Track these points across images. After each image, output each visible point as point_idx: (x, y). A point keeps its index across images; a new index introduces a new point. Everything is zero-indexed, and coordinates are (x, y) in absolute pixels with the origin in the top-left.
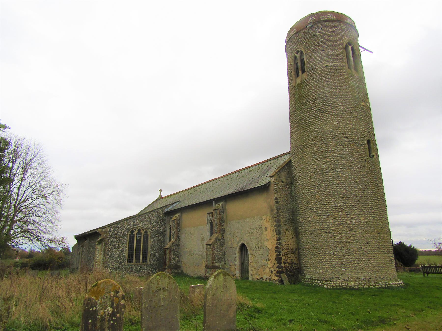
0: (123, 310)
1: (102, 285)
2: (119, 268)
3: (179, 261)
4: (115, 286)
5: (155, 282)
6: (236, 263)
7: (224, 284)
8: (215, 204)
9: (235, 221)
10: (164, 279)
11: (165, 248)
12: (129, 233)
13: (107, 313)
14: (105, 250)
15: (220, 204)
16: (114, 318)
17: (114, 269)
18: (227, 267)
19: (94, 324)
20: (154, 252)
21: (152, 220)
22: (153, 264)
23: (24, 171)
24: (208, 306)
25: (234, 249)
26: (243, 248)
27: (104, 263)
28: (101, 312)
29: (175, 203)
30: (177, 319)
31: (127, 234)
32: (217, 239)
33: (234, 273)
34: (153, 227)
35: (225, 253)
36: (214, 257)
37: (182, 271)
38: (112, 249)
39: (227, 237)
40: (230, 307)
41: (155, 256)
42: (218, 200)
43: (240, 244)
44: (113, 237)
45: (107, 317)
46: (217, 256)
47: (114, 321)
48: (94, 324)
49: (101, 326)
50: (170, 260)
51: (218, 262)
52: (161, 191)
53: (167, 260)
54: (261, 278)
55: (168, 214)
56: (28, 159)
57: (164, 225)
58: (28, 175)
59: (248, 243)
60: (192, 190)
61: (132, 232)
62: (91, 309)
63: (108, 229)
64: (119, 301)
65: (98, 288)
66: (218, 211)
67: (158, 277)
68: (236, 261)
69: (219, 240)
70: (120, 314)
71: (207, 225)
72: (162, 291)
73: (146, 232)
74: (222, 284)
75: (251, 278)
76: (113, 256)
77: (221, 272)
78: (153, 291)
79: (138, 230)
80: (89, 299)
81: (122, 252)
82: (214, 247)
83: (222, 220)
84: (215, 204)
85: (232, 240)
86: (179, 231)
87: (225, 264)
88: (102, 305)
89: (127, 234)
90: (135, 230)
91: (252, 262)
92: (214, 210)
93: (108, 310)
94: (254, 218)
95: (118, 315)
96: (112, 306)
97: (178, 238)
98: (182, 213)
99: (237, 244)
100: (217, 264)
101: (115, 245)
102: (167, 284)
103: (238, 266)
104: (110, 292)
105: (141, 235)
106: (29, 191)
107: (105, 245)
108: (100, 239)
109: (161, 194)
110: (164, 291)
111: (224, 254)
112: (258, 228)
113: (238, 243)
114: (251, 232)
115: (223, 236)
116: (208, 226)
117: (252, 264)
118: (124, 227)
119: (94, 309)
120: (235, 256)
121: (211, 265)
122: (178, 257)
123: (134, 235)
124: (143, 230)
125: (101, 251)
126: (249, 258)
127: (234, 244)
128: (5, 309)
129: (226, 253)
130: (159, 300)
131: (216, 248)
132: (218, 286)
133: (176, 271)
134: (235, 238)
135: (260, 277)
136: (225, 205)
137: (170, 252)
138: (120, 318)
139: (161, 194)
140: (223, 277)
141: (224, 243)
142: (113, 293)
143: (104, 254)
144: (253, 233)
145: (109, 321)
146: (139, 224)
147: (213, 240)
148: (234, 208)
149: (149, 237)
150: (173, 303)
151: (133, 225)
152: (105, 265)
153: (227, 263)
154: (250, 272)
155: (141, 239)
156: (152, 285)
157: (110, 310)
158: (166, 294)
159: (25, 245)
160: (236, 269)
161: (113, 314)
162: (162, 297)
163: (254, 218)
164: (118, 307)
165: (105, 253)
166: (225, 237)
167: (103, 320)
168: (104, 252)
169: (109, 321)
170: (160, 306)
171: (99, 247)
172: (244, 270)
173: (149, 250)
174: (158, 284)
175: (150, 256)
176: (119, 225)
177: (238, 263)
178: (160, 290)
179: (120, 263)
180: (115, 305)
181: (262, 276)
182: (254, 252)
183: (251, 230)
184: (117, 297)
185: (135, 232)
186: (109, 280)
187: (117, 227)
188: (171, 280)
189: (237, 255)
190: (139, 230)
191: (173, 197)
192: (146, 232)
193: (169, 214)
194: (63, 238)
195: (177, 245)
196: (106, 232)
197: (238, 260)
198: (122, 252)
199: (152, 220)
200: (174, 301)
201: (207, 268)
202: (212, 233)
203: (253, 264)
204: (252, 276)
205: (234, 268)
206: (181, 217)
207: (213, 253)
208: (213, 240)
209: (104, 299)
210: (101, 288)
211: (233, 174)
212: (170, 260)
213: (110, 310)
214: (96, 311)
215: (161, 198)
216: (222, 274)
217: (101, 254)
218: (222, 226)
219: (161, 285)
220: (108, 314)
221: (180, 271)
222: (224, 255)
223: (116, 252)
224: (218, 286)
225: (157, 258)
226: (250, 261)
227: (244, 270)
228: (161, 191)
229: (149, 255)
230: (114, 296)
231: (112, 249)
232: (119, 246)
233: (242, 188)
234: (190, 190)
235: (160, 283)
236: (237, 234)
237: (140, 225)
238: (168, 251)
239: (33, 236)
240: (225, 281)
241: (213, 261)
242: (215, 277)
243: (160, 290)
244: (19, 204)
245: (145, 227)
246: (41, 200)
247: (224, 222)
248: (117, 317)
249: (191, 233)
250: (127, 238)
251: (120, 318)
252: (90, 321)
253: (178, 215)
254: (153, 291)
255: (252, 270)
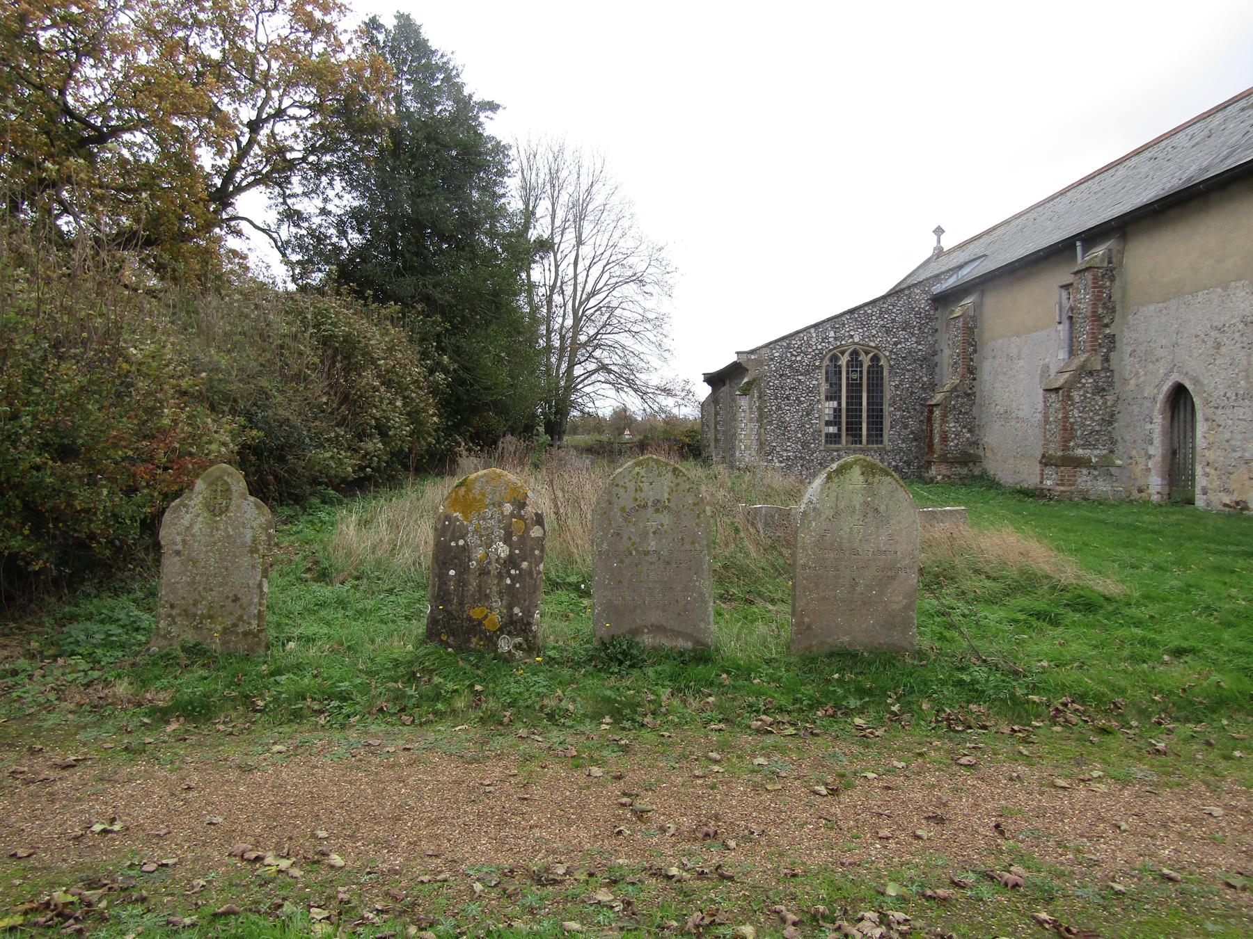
0: (537, 552)
1: (478, 486)
2: (801, 458)
3: (976, 443)
4: (515, 489)
5: (628, 484)
6: (1152, 451)
7: (866, 503)
8: (1085, 251)
9: (1152, 307)
10: (660, 475)
11: (930, 403)
12: (826, 362)
13: (494, 558)
14: (759, 408)
15: (1100, 251)
16: (513, 572)
17: (788, 458)
18: (1119, 462)
19: (461, 581)
20: (903, 417)
21: (894, 321)
22: (901, 450)
23: (580, 218)
24: (804, 566)
25: (1147, 404)
26: (1179, 398)
27: (761, 444)
28: (480, 553)
29: (966, 263)
30: (702, 595)
31: (819, 367)
32: (1085, 371)
33: (1141, 483)
34: (896, 344)
35: (1112, 415)
36: (1068, 433)
37: (985, 472)
38: (779, 408)
39: (1126, 363)
40: (893, 578)
41: (906, 426)
42: (1091, 237)
43: (1167, 387)
44: (781, 376)
45: (494, 567)
46: (1083, 425)
47: (512, 577)
48: (461, 581)
49: (480, 586)
50: (944, 439)
51: (1083, 446)
52: (939, 231)
53: (937, 440)
54: (1237, 503)
55: (944, 304)
56: (584, 187)
57: (932, 335)
58: (587, 227)
59: (1196, 381)
60: (1031, 216)
61: (834, 358)
62: (453, 544)
63: (766, 354)
64: (527, 529)
65: (469, 490)
66: (1089, 276)
67: (637, 469)
68: (1151, 442)
69: (1091, 373)
70: (530, 563)
71: (1060, 327)
72: (650, 510)
73: (876, 359)
74: (858, 501)
75: (1200, 501)
76: (783, 426)
77: (855, 462)
78: (623, 509)
79: (851, 354)
80: (448, 517)
81: (808, 415)
82: (1070, 398)
83: (1105, 306)
84: (1085, 251)
85: (1142, 372)
86: (975, 351)
87: (1112, 452)
88: (481, 536)
89: (819, 367)
90: (843, 353)
91: (1210, 446)
92: (1076, 273)
93: (496, 550)
94: (1226, 288)
95: (525, 565)
96: (507, 540)
97: (972, 373)
98: (983, 293)
99: (1158, 386)
100: (1080, 452)
101: (788, 398)
102: (667, 490)
103: (1158, 458)
104: (500, 505)
105: (861, 366)
106: (596, 271)
107: (760, 397)
108: (746, 380)
109: (939, 241)
110: (657, 511)
111: (1110, 420)
112: (1241, 326)
113: (1164, 380)
114: (1210, 343)
115: (1106, 359)
116: (1063, 329)
117: (1207, 453)
118: (810, 346)
119: (461, 542)
120: (1149, 426)
121: (1060, 454)
122: (970, 431)
123: (840, 367)
124: (867, 353)
125: (751, 413)
126: (1199, 434)
127: (1145, 385)
128: (260, 526)
129: (1118, 416)
130: (644, 535)
131: (1077, 399)
132: (842, 505)
133: (965, 471)
134: (1151, 367)
135: (1236, 497)
136: (1122, 252)
137: (944, 416)
138: (530, 573)
139: (939, 241)
140: (861, 478)
141: (1111, 384)
142: (508, 508)
143: (760, 420)
144: (1218, 346)
145: (500, 576)
146: (852, 336)
147: (1067, 375)
148: (1154, 259)
149: (886, 373)
150: (688, 546)
151: (836, 339)
152: (765, 450)
153: (1120, 448)
154: (1201, 482)
155: (861, 378)
156: (621, 491)
157: (503, 550)
158: (665, 519)
159: (602, 400)
160: (1148, 470)
161: (511, 561)
162: (652, 525)
163: (1226, 288)
164: (524, 543)
165: (762, 417)
166: (1113, 364)
167: (484, 572)
168: (760, 415)
169: (500, 576)
170: (646, 553)
171: (744, 402)
172: (1178, 469)
173: (887, 409)
174: (638, 489)
175: (892, 427)
176: (796, 342)
177: (1157, 449)
178: (645, 507)
179: (805, 445)
180: (515, 538)
181: (1243, 497)
182: (1220, 412)
183: (1213, 333)
184: (521, 517)
185: (844, 361)
186: (498, 471)
187: (788, 347)
188: (680, 480)
189: (1157, 425)
190: (855, 354)
191: (971, 246)
192: (876, 359)
193: (944, 300)
194: (687, 382)
195: (968, 392)
196: (759, 363)
197: (1157, 440)
198: (808, 415)
199: (894, 321)
200: (693, 543)
201: (1046, 465)
202: (1072, 353)
203: (1211, 455)
204: (1205, 493)
205: (1141, 466)
206: (978, 307)
207: (1066, 418)
208: (1067, 375)
209: (484, 519)
210: (476, 491)
211: (1180, 134)
212: (944, 439)
213: (503, 550)
214: (465, 549)
215: (939, 253)
216: (856, 471)
217: (751, 420)
218: (1107, 326)
219: (649, 494)
220: (497, 561)
221: (977, 472)
222: (1110, 423)
223: (791, 416)
224: (842, 505)
225: (912, 432)
226: (1200, 442)
227: (1178, 469)
228: (939, 231)
229: (887, 423)
230: (512, 515)
231: (779, 408)
232: (798, 399)
233: (1189, 179)
234: (1024, 217)
235: (645, 486)
236: (1160, 353)
237: (856, 340)
238: (937, 412)
239: (625, 379)
240: (870, 489)
241: (1066, 441)
242: (829, 477)
243: (645, 507)
244: (581, 304)
245: (872, 344)
246: (630, 290)
247: (1113, 310)
248: (521, 570)
249: (1010, 358)
250: (821, 375)
251: (530, 573)
252: (452, 572)
253: (968, 301)
254: (623, 509)
255: (1207, 475)
